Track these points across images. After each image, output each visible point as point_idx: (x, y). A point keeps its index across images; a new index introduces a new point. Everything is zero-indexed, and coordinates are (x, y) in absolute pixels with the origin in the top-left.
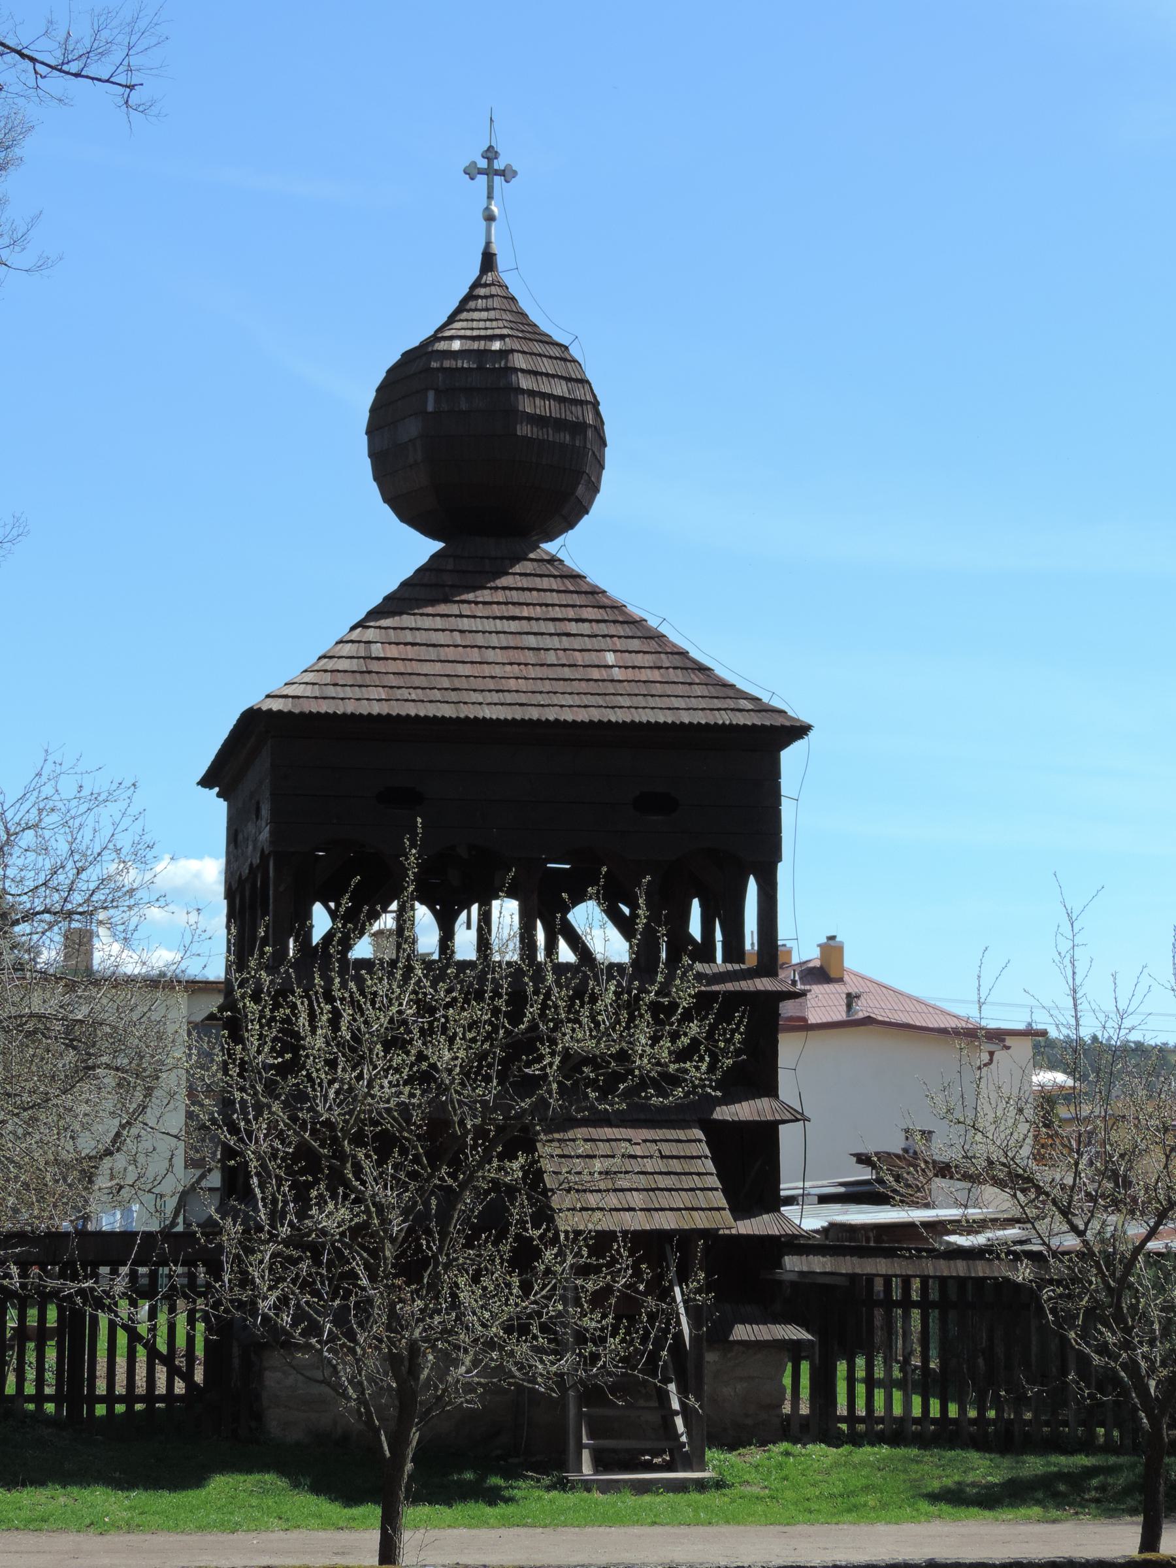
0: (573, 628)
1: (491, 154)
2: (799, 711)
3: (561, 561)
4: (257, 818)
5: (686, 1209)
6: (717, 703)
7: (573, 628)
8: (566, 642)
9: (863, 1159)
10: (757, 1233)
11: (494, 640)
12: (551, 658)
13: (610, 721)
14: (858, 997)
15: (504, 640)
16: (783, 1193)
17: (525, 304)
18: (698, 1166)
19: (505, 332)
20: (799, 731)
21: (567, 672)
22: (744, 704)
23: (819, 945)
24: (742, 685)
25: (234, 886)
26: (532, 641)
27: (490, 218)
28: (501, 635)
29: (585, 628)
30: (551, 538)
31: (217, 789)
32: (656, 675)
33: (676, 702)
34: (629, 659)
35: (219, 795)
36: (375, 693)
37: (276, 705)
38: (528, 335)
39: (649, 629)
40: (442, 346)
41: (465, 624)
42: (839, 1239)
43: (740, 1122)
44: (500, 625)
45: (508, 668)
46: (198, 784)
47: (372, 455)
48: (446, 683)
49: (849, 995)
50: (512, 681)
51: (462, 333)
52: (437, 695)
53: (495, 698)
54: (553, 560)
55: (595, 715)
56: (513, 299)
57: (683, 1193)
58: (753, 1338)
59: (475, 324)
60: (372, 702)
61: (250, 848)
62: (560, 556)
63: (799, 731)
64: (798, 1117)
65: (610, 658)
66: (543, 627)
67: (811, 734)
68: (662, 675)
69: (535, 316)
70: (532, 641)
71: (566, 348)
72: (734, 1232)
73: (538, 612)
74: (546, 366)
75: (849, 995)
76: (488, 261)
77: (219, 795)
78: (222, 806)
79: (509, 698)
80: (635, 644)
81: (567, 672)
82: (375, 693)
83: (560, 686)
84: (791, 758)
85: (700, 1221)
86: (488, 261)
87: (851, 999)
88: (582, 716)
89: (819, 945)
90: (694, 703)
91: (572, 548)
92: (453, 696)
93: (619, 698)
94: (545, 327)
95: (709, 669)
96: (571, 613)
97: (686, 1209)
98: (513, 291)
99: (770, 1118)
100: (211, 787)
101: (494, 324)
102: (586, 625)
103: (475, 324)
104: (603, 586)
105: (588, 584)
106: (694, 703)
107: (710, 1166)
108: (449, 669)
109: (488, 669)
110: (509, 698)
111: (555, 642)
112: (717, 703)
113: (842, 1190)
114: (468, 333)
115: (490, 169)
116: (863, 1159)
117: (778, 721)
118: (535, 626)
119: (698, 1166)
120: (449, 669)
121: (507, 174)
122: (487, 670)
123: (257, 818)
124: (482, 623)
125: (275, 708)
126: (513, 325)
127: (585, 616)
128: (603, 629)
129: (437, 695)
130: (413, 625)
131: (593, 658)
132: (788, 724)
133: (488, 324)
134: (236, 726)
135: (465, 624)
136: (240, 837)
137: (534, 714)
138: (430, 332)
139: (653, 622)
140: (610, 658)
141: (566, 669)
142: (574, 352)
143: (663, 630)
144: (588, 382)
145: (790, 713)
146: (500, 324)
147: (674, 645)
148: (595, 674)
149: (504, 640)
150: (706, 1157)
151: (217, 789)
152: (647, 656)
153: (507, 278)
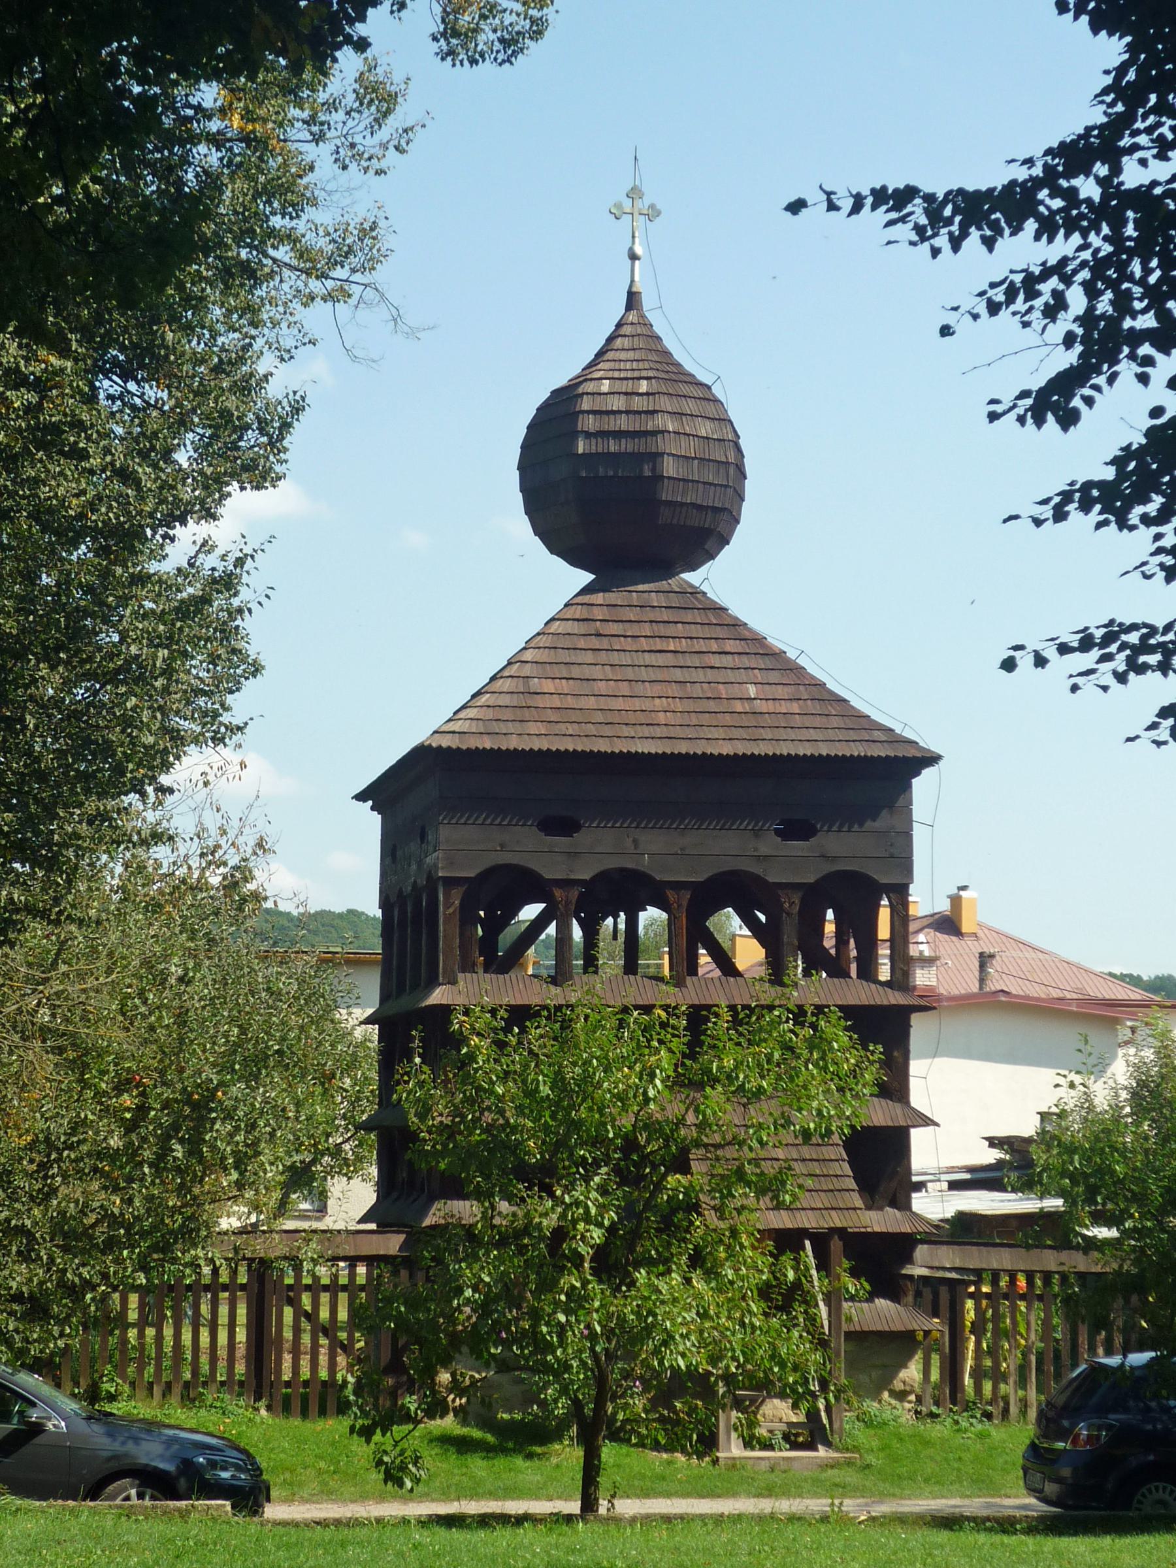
0: (715, 660)
1: (634, 193)
2: (929, 742)
3: (704, 593)
4: (422, 842)
5: (826, 1209)
6: (852, 735)
7: (715, 660)
8: (710, 675)
9: (993, 1142)
10: (890, 1231)
11: (644, 674)
12: (697, 691)
13: (753, 754)
14: (992, 956)
15: (653, 674)
16: (915, 1179)
17: (670, 343)
18: (835, 1168)
19: (651, 374)
20: (932, 759)
21: (712, 706)
22: (877, 735)
23: (949, 897)
24: (876, 716)
25: (393, 899)
26: (678, 675)
27: (633, 257)
28: (650, 669)
29: (727, 661)
30: (693, 568)
31: (370, 803)
32: (795, 707)
33: (813, 734)
34: (770, 691)
35: (372, 809)
36: (533, 728)
37: (445, 742)
38: (674, 377)
39: (789, 660)
40: (590, 387)
41: (615, 658)
42: (966, 1228)
43: (875, 1127)
44: (649, 659)
45: (657, 701)
46: (361, 797)
47: (523, 490)
48: (599, 717)
49: (981, 955)
50: (661, 715)
51: (610, 374)
52: (591, 729)
53: (646, 731)
54: (696, 592)
55: (741, 748)
56: (659, 338)
57: (822, 1194)
58: (887, 1329)
59: (622, 365)
60: (532, 737)
61: (414, 867)
62: (703, 588)
63: (932, 759)
64: (927, 1121)
65: (752, 691)
66: (690, 660)
67: (941, 763)
68: (800, 707)
69: (679, 355)
70: (678, 675)
71: (709, 388)
72: (869, 1230)
73: (684, 645)
74: (690, 406)
75: (981, 955)
76: (633, 300)
77: (372, 809)
78: (376, 818)
79: (659, 731)
80: (774, 677)
81: (712, 706)
82: (533, 728)
83: (706, 719)
84: (923, 785)
85: (836, 1220)
86: (633, 300)
87: (984, 960)
88: (726, 749)
89: (949, 897)
90: (831, 734)
91: (716, 578)
92: (607, 731)
93: (762, 730)
94: (689, 366)
95: (845, 701)
96: (714, 646)
97: (826, 1209)
98: (658, 329)
99: (903, 1123)
100: (365, 801)
101: (641, 365)
102: (729, 657)
103: (622, 365)
104: (744, 618)
105: (730, 616)
106: (831, 734)
107: (846, 1167)
108: (603, 703)
109: (648, 718)
110: (659, 731)
111: (700, 675)
112: (852, 735)
113: (967, 1176)
114: (616, 374)
115: (637, 206)
116: (993, 1142)
117: (911, 753)
118: (681, 660)
119: (835, 1168)
120: (603, 703)
121: (653, 213)
122: (637, 704)
123: (422, 842)
124: (632, 657)
125: (444, 745)
126: (658, 366)
127: (728, 649)
128: (746, 661)
129: (591, 729)
130: (568, 660)
131: (735, 691)
132: (919, 755)
133: (635, 365)
134: (404, 757)
135: (615, 658)
136: (399, 853)
137: (683, 748)
138: (577, 370)
139: (791, 654)
140: (752, 691)
141: (711, 702)
142: (717, 391)
143: (800, 661)
144: (730, 421)
145: (922, 744)
146: (647, 365)
147: (813, 677)
148: (738, 706)
149: (653, 674)
150: (843, 1160)
151: (370, 803)
152: (786, 689)
153: (652, 317)
